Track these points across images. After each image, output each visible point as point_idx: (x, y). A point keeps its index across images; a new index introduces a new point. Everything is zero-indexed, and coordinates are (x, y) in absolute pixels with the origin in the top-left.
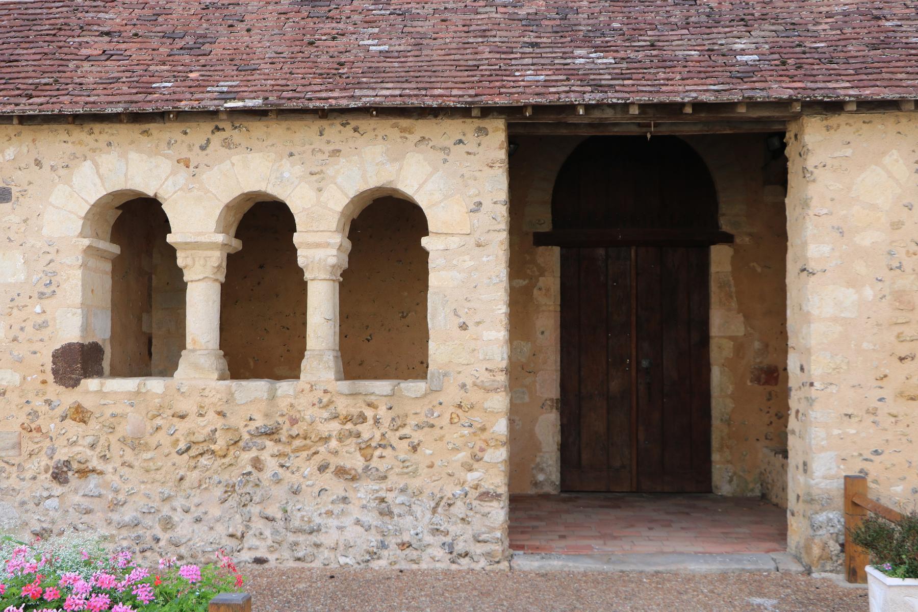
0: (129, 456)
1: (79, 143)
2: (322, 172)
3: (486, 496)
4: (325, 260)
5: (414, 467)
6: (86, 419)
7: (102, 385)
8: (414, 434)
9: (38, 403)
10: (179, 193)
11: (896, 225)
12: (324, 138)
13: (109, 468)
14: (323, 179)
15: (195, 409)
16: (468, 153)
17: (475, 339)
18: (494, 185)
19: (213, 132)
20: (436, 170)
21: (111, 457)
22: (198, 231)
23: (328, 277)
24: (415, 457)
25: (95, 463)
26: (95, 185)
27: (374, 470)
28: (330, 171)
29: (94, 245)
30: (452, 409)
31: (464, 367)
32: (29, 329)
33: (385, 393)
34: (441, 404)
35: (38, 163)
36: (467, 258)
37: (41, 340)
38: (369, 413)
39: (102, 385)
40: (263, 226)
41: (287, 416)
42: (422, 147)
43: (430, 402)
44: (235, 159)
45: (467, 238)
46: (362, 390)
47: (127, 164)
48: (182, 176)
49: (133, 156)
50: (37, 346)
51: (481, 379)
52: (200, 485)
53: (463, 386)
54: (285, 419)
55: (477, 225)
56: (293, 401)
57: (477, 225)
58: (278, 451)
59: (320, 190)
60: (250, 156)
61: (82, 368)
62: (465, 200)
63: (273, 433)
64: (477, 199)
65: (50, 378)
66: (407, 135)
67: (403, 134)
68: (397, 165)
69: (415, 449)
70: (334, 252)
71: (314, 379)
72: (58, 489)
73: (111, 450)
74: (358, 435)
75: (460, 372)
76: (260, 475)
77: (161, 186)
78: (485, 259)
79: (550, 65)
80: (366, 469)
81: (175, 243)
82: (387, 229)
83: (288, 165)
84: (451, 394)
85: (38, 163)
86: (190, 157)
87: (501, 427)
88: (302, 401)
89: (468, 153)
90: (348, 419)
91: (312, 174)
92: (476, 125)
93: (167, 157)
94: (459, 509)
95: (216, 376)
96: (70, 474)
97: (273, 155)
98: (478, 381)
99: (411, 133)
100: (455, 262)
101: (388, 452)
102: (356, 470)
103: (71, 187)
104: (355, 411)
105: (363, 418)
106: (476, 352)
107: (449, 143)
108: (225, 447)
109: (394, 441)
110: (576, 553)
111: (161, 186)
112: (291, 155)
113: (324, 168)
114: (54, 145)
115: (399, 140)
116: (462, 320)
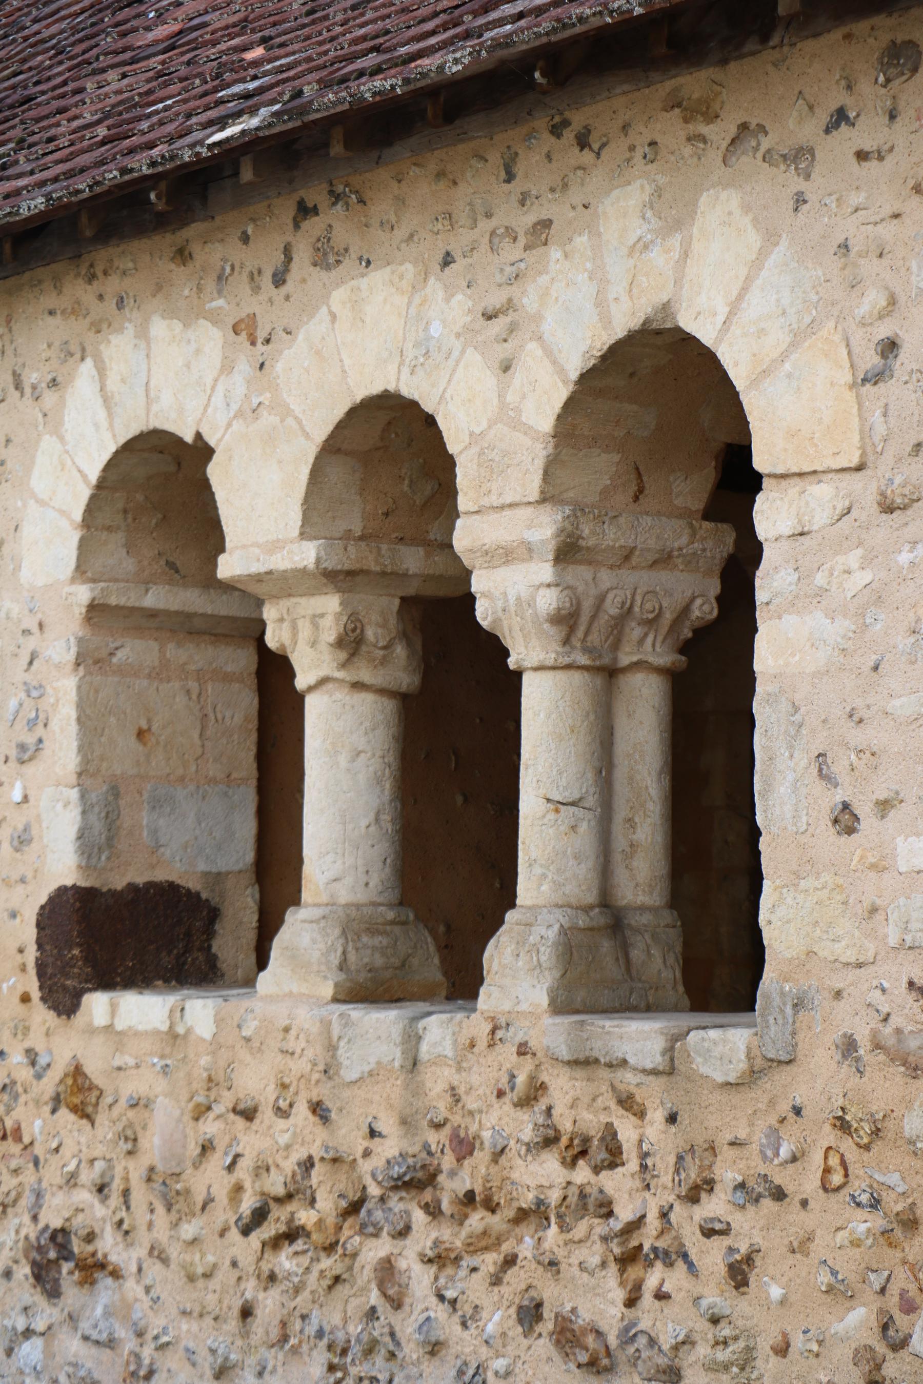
1: (73, 312)
2: (509, 306)
4: (531, 603)
5: (741, 1344)
6: (89, 1109)
7: (114, 1009)
8: (737, 1220)
10: (236, 425)
12: (517, 187)
14: (512, 328)
15: (271, 1093)
16: (862, 156)
17: (873, 867)
19: (297, 226)
20: (771, 238)
21: (728, 1224)
23: (550, 658)
24: (741, 1309)
26: (96, 426)
27: (642, 1341)
28: (529, 301)
29: (113, 601)
30: (829, 1136)
31: (852, 975)
33: (649, 1066)
34: (797, 1111)
36: (853, 559)
37: (23, 880)
38: (627, 1132)
39: (114, 1009)
41: (447, 1131)
42: (745, 162)
43: (772, 1103)
44: (339, 296)
45: (855, 482)
46: (597, 1048)
47: (149, 347)
51: (895, 1021)
52: (285, 1338)
53: (849, 1046)
54: (444, 1135)
55: (880, 429)
56: (456, 1079)
57: (880, 429)
58: (436, 1243)
59: (506, 368)
60: (364, 283)
61: (86, 960)
64: (883, 331)
65: (32, 985)
66: (704, 129)
67: (691, 128)
68: (675, 241)
69: (739, 1274)
70: (545, 571)
71: (507, 1006)
73: (133, 1204)
74: (606, 1210)
75: (838, 994)
76: (396, 1319)
77: (205, 410)
78: (904, 558)
79: (17, 192)
80: (628, 1336)
81: (232, 577)
83: (441, 294)
84: (819, 1081)
86: (257, 310)
88: (475, 1079)
89: (862, 156)
90: (578, 1152)
91: (489, 316)
92: (885, 38)
93: (214, 318)
95: (328, 990)
96: (66, 1267)
97: (409, 269)
98: (888, 1030)
99: (712, 117)
100: (820, 579)
101: (675, 1279)
102: (599, 1333)
103: (62, 439)
104: (591, 1122)
105: (614, 1156)
106: (880, 916)
107: (808, 130)
108: (331, 1220)
109: (693, 1241)
111: (205, 410)
112: (447, 260)
113: (514, 291)
115: (688, 150)
116: (839, 796)
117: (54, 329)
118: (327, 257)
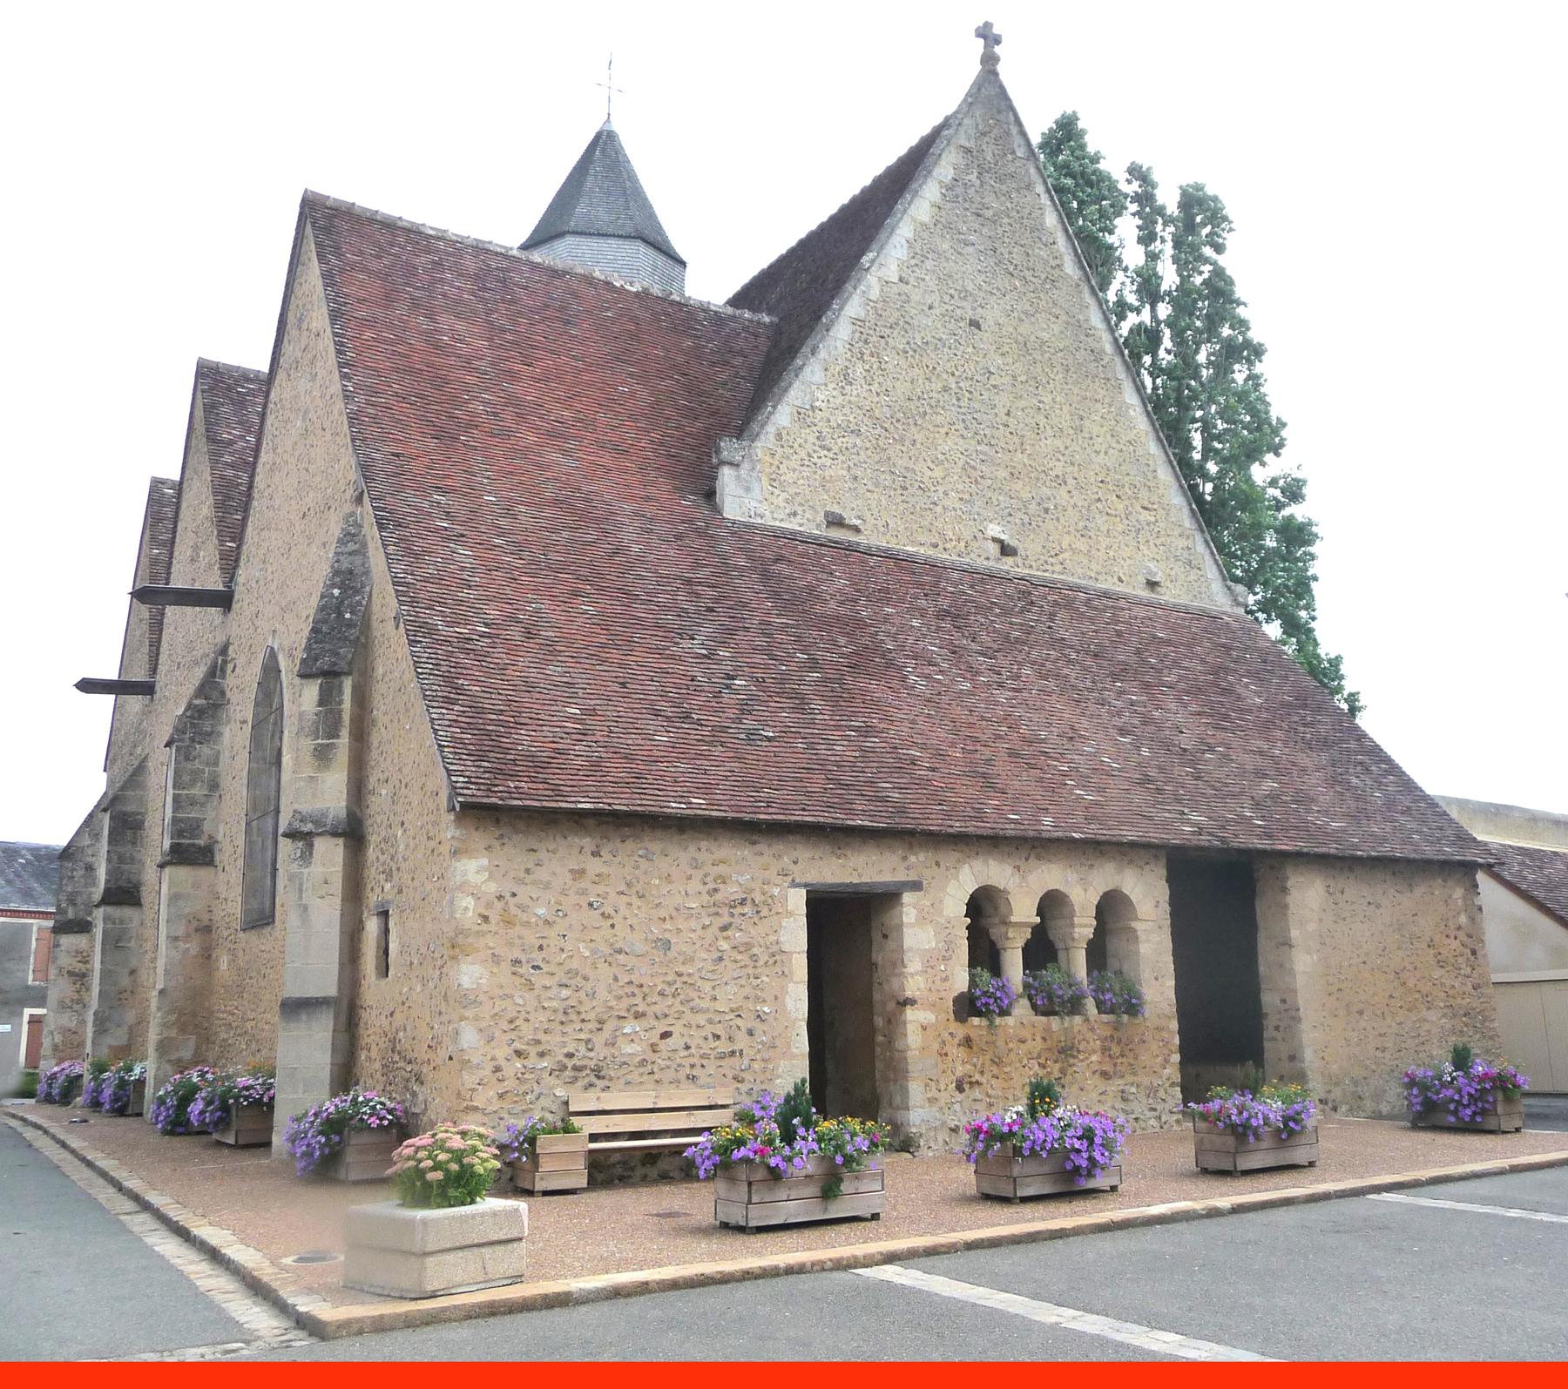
0: (995, 1070)
3: (1173, 1085)
9: (946, 1035)
11: (1321, 920)
13: (984, 1080)
18: (1162, 891)
22: (1024, 911)
25: (977, 1077)
32: (938, 983)
35: (938, 864)
40: (1051, 904)
48: (1017, 879)
49: (991, 862)
50: (943, 994)
62: (1148, 897)
63: (206, 930)
65: (952, 1017)
72: (959, 1097)
82: (1111, 908)
85: (938, 864)
87: (1177, 1040)
94: (1161, 1094)
110: (1101, 1341)
114: (949, 857)
117: (956, 855)
118: (1039, 858)
